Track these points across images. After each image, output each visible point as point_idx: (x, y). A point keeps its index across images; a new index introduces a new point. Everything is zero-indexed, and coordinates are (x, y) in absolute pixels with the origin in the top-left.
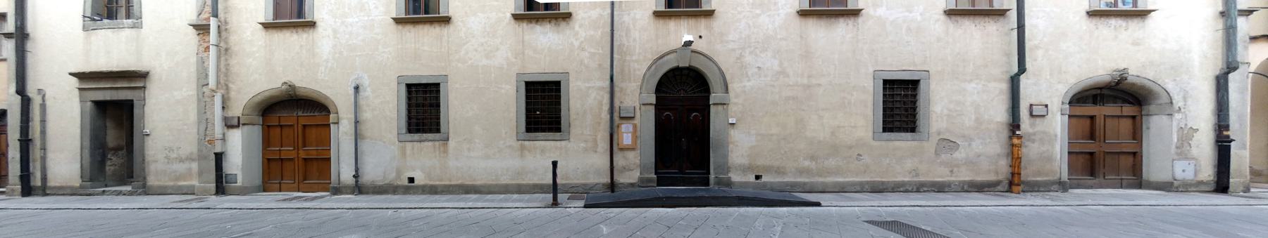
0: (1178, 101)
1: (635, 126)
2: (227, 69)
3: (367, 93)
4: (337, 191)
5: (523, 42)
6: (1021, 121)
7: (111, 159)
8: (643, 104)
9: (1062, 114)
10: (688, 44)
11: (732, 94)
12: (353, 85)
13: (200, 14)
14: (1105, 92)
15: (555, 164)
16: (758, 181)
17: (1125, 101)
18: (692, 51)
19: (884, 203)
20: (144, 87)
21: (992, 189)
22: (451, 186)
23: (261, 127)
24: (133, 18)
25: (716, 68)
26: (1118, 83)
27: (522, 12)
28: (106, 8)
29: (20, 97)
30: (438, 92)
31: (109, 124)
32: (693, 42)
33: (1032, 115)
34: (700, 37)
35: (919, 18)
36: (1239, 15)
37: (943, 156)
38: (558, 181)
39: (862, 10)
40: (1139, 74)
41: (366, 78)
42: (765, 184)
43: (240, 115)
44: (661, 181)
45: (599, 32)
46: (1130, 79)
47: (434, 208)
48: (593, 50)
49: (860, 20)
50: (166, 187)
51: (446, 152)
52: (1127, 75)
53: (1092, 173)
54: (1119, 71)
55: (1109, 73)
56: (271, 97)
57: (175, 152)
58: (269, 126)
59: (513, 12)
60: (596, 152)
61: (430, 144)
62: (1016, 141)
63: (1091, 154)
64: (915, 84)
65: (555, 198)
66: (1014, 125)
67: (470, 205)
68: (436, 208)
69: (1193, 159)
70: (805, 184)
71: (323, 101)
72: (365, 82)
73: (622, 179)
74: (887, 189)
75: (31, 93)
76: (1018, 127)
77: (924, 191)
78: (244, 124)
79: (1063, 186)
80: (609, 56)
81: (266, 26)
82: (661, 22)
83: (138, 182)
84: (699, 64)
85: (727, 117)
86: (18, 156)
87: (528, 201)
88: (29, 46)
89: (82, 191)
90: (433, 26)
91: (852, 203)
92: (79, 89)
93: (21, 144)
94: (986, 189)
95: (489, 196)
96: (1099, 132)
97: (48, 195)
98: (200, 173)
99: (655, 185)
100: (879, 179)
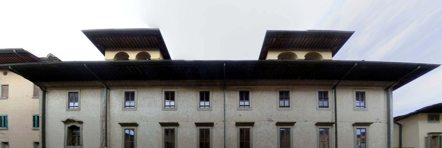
13: (101, 146)
24: (80, 146)
28: (71, 142)
33: (125, 129)
86: (35, 124)
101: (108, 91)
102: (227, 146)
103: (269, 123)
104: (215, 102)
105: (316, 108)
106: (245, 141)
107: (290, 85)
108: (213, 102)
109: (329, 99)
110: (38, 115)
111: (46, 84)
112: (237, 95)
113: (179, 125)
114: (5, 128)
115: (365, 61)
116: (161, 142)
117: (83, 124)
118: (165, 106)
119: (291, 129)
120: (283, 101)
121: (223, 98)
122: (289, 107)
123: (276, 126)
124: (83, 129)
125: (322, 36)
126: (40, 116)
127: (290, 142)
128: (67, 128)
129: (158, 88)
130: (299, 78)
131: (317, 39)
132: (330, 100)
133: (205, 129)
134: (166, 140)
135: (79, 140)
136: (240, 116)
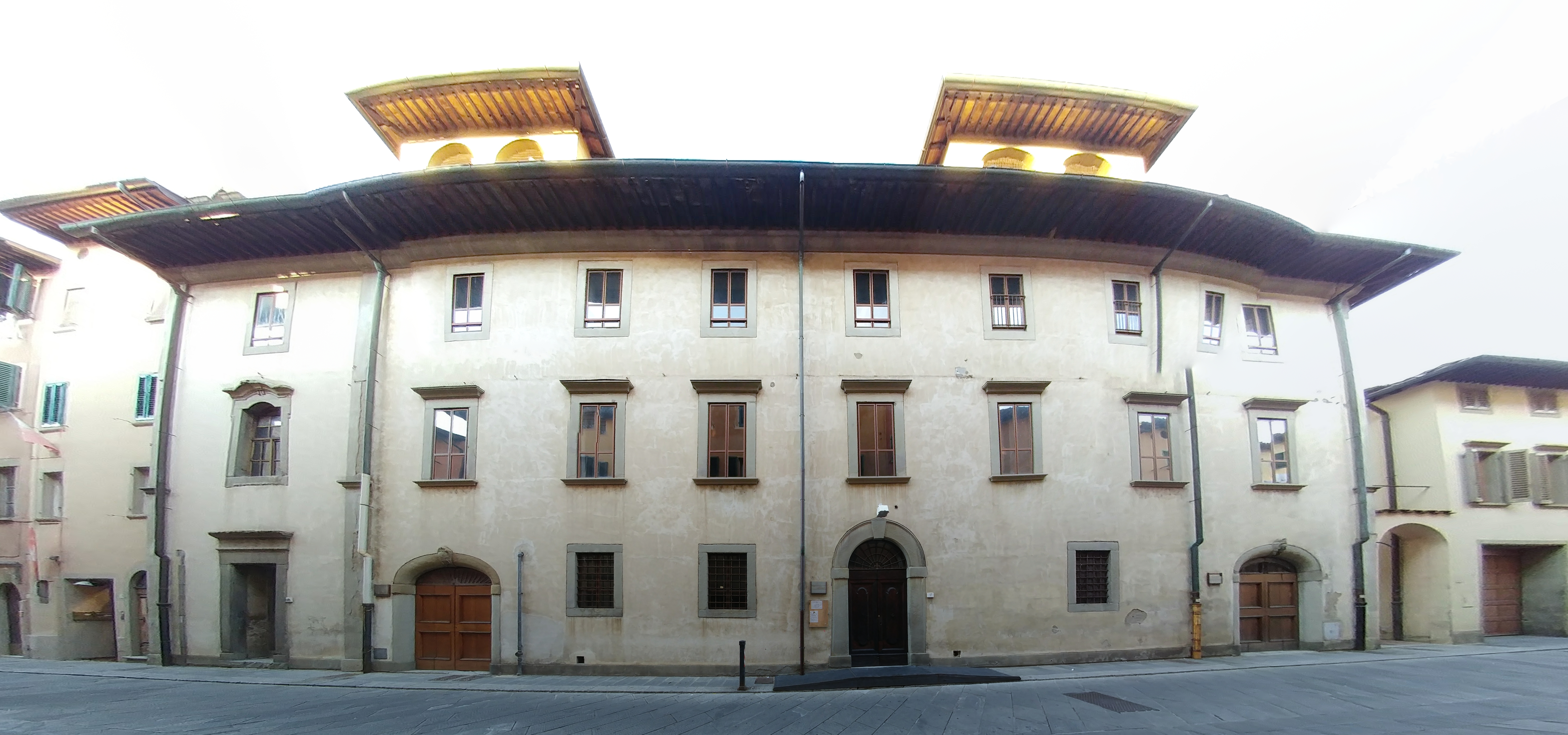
0: (1326, 570)
1: (825, 603)
2: (378, 532)
3: (533, 561)
4: (499, 669)
5: (706, 509)
6: (1200, 589)
7: (252, 628)
8: (836, 579)
9: (1234, 582)
10: (883, 514)
11: (929, 567)
12: (518, 553)
14: (1269, 561)
15: (742, 644)
16: (957, 657)
17: (1284, 569)
18: (887, 522)
19: (1080, 674)
20: (288, 550)
21: (1176, 656)
22: (624, 666)
23: (414, 597)
25: (912, 540)
26: (1279, 552)
27: (706, 478)
29: (158, 558)
30: (612, 562)
31: (250, 590)
32: (888, 512)
33: (1209, 584)
34: (896, 507)
35: (1108, 490)
36: (1368, 492)
37: (1132, 625)
38: (746, 663)
39: (1046, 475)
40: (1295, 544)
41: (532, 545)
42: (964, 661)
43: (392, 584)
44: (856, 661)
45: (789, 501)
46: (1288, 549)
47: (606, 692)
48: (782, 521)
49: (1045, 484)
50: (310, 661)
51: (619, 628)
52: (1285, 545)
53: (1260, 637)
54: (1279, 542)
55: (1271, 543)
56: (426, 564)
57: (320, 622)
58: (422, 596)
59: (695, 478)
60: (785, 631)
61: (602, 619)
62: (1195, 609)
63: (1259, 619)
64: (1106, 554)
65: (742, 682)
66: (1194, 594)
67: (647, 688)
68: (609, 692)
69: (1339, 621)
70: (1003, 658)
71: (486, 572)
72: (531, 550)
73: (812, 660)
74: (1081, 660)
75: (170, 554)
76: (1198, 596)
77: (1116, 661)
78: (394, 594)
79: (1235, 651)
80: (800, 526)
81: (423, 485)
82: (855, 490)
83: (280, 654)
84: (894, 535)
85: (925, 590)
87: (711, 685)
88: (171, 502)
89: (222, 662)
90: (607, 490)
91: (1051, 676)
92: (220, 551)
93: (160, 608)
94: (1171, 656)
95: (668, 679)
96: (1264, 598)
97: (188, 665)
98: (347, 647)
99: (851, 665)
100: (1074, 651)
101: (386, 282)
102: (812, 468)
103: (958, 383)
104: (768, 305)
105: (1109, 334)
106: (877, 450)
107: (1023, 254)
108: (761, 308)
109: (1142, 306)
110: (154, 376)
111: (191, 273)
112: (846, 284)
113: (632, 388)
114: (57, 425)
115: (1230, 196)
116: (564, 455)
117: (293, 397)
118: (585, 321)
119: (1033, 405)
120: (1004, 309)
121: (797, 292)
122: (1023, 328)
123: (986, 395)
124: (291, 416)
125: (1113, 106)
126: (161, 376)
127: (1031, 452)
128: (239, 413)
129: (564, 257)
130: (1053, 232)
131: (1097, 113)
132: (1144, 309)
133: (727, 403)
134: (583, 450)
135: (275, 451)
136: (859, 356)
